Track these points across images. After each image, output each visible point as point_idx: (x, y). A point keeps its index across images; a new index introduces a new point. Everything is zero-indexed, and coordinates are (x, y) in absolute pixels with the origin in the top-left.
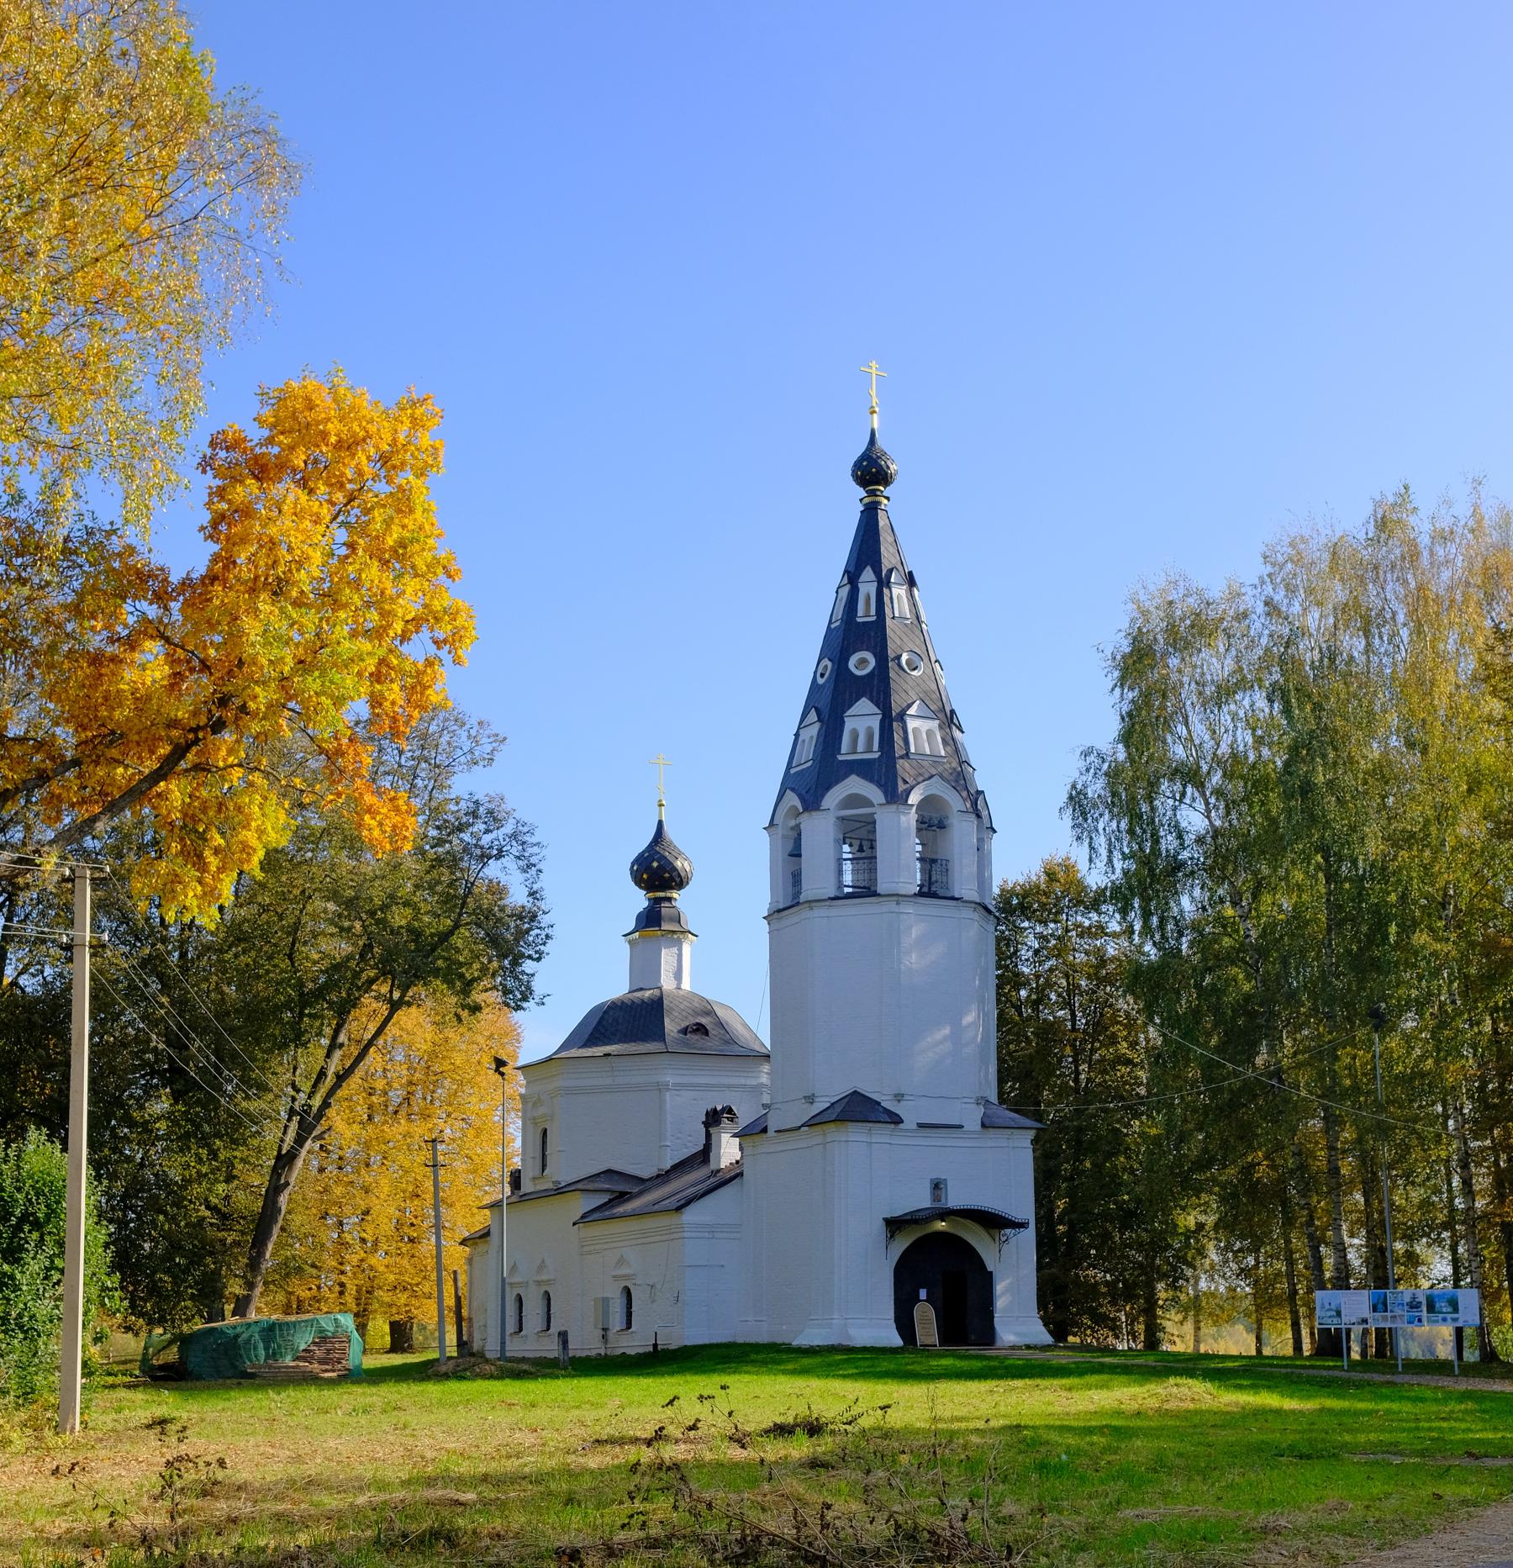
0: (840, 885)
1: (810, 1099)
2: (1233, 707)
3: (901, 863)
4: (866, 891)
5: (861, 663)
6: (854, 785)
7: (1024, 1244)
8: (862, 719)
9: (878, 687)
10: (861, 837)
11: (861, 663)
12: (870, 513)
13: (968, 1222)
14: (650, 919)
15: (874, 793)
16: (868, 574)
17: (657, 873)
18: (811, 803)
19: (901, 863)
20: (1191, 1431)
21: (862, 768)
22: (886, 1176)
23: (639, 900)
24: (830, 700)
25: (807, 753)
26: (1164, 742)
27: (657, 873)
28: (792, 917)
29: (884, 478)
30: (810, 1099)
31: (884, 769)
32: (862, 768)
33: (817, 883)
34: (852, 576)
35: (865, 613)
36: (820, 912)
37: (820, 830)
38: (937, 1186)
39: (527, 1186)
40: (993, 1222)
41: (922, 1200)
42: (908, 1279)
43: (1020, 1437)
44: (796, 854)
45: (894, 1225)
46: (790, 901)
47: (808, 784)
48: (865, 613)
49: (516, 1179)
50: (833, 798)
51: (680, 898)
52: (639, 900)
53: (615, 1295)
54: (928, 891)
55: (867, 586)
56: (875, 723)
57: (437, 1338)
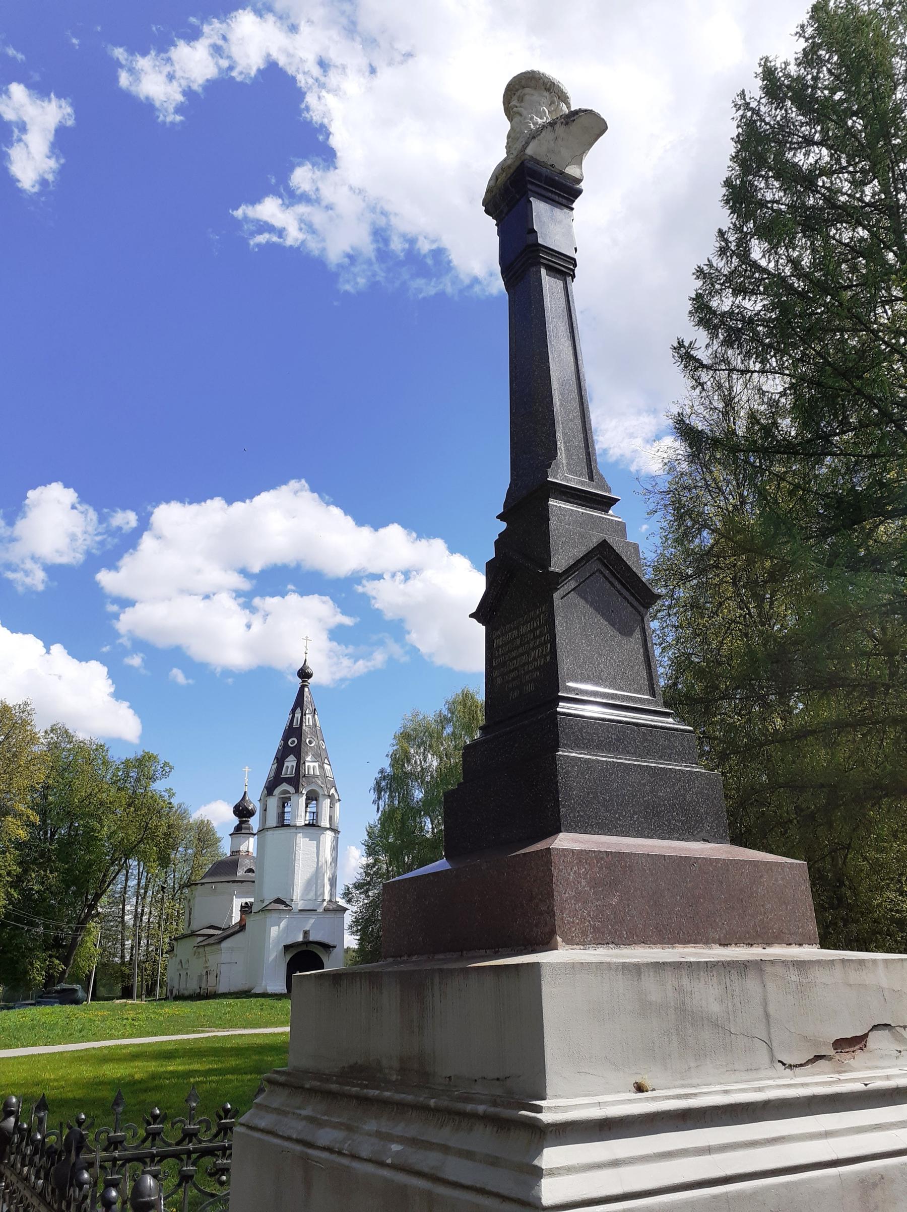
5: (292, 742)
8: (290, 763)
9: (297, 752)
11: (292, 742)
12: (302, 688)
13: (321, 948)
15: (291, 789)
16: (299, 710)
20: (531, 636)
21: (288, 781)
25: (272, 774)
26: (407, 785)
29: (309, 676)
30: (263, 901)
32: (288, 781)
34: (293, 711)
35: (296, 724)
36: (270, 832)
38: (306, 933)
43: (768, 943)
44: (265, 810)
45: (287, 948)
48: (296, 724)
50: (277, 792)
52: (236, 821)
53: (204, 973)
55: (298, 715)
56: (294, 764)
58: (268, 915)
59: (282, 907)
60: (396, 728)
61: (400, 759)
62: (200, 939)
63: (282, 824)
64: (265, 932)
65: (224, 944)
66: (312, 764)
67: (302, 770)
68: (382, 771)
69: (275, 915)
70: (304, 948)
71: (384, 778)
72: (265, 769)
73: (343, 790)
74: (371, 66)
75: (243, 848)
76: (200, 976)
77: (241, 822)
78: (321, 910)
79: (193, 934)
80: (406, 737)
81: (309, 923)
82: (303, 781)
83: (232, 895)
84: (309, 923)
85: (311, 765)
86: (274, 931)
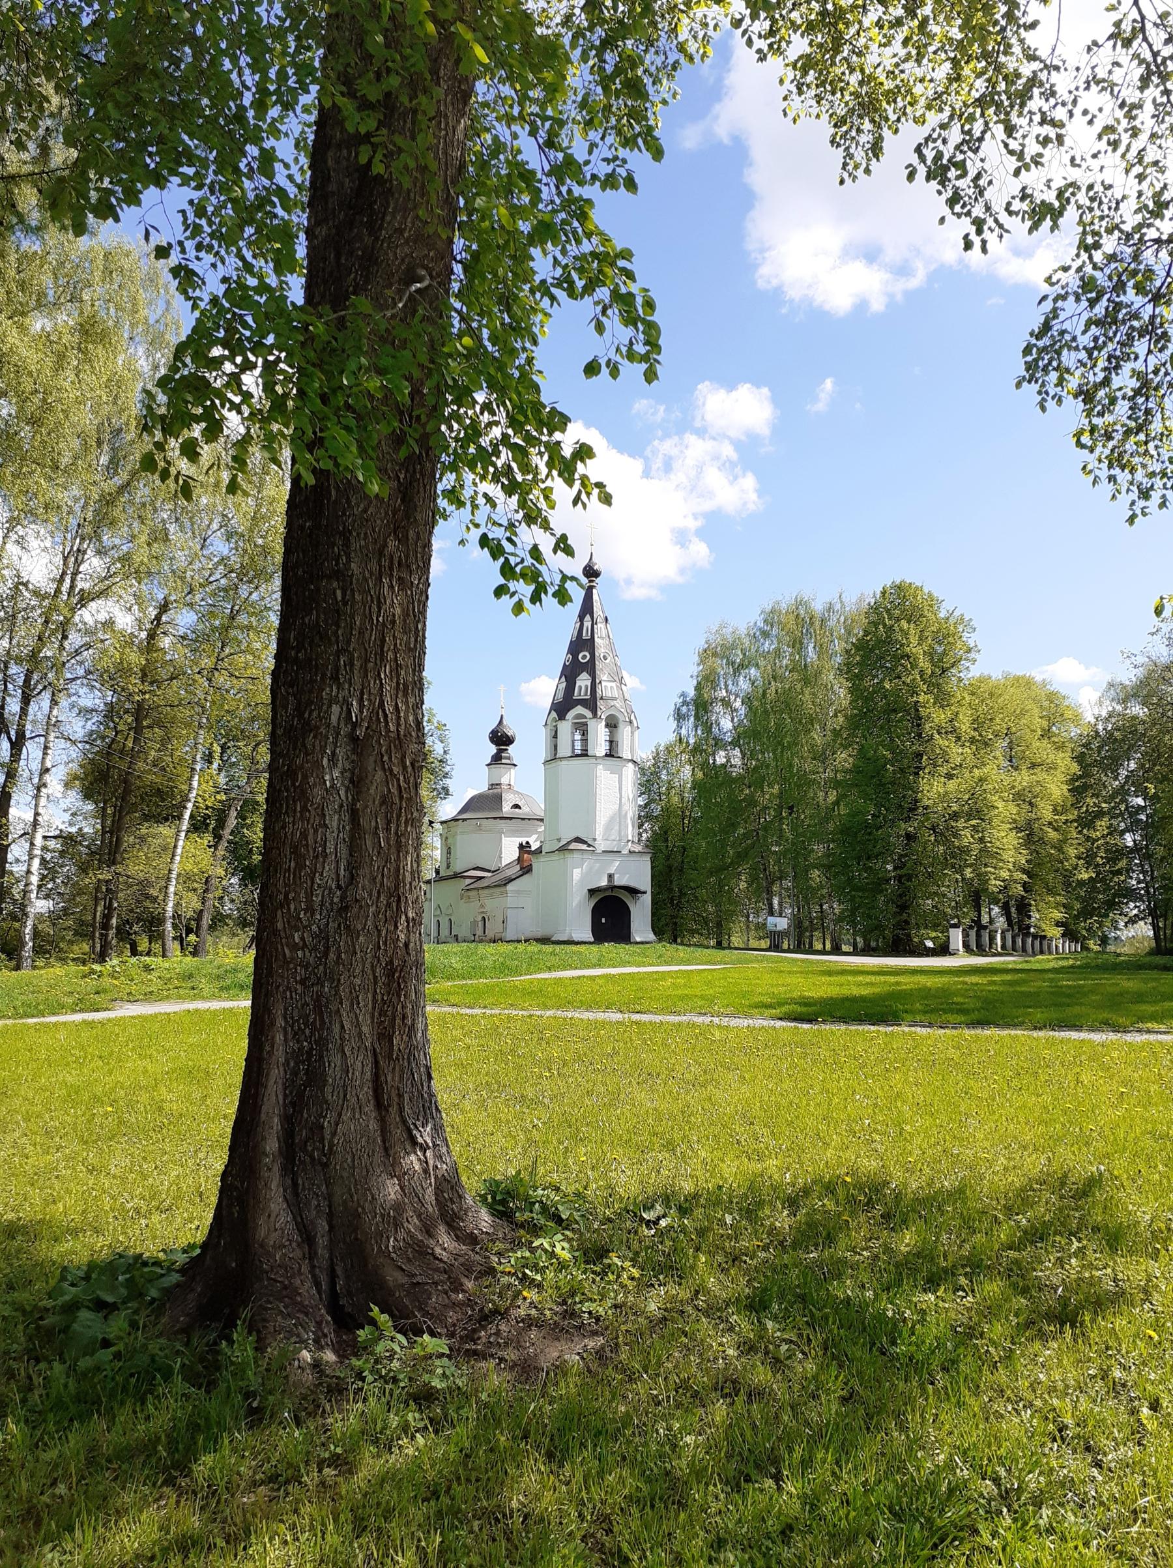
0: (573, 749)
1: (559, 840)
2: (1091, 378)
3: (599, 746)
4: (584, 754)
6: (579, 710)
7: (647, 899)
8: (583, 681)
10: (582, 728)
14: (497, 759)
15: (588, 714)
16: (588, 617)
17: (501, 739)
18: (562, 716)
19: (599, 746)
22: (582, 876)
23: (493, 749)
24: (570, 673)
25: (560, 695)
27: (501, 739)
28: (553, 764)
29: (509, 741)
30: (559, 840)
31: (591, 704)
33: (564, 750)
34: (581, 618)
37: (565, 727)
38: (610, 876)
39: (442, 873)
40: (633, 892)
41: (604, 883)
42: (597, 912)
44: (555, 736)
45: (592, 892)
46: (554, 758)
47: (561, 708)
48: (586, 635)
49: (437, 872)
50: (571, 715)
51: (511, 749)
52: (493, 749)
54: (610, 755)
55: (587, 623)
56: (589, 683)
57: (463, 931)
58: (569, 856)
59: (584, 847)
60: (701, 644)
61: (707, 681)
62: (468, 881)
63: (584, 754)
64: (566, 875)
65: (510, 887)
66: (609, 685)
67: (599, 691)
68: (683, 695)
69: (576, 855)
70: (609, 893)
71: (685, 703)
72: (547, 688)
73: (641, 719)
74: (1108, 9)
75: (504, 781)
76: (474, 923)
77: (500, 751)
78: (625, 852)
79: (456, 876)
80: (708, 654)
81: (614, 866)
82: (600, 703)
83: (501, 833)
84: (614, 866)
85: (607, 687)
86: (577, 873)
